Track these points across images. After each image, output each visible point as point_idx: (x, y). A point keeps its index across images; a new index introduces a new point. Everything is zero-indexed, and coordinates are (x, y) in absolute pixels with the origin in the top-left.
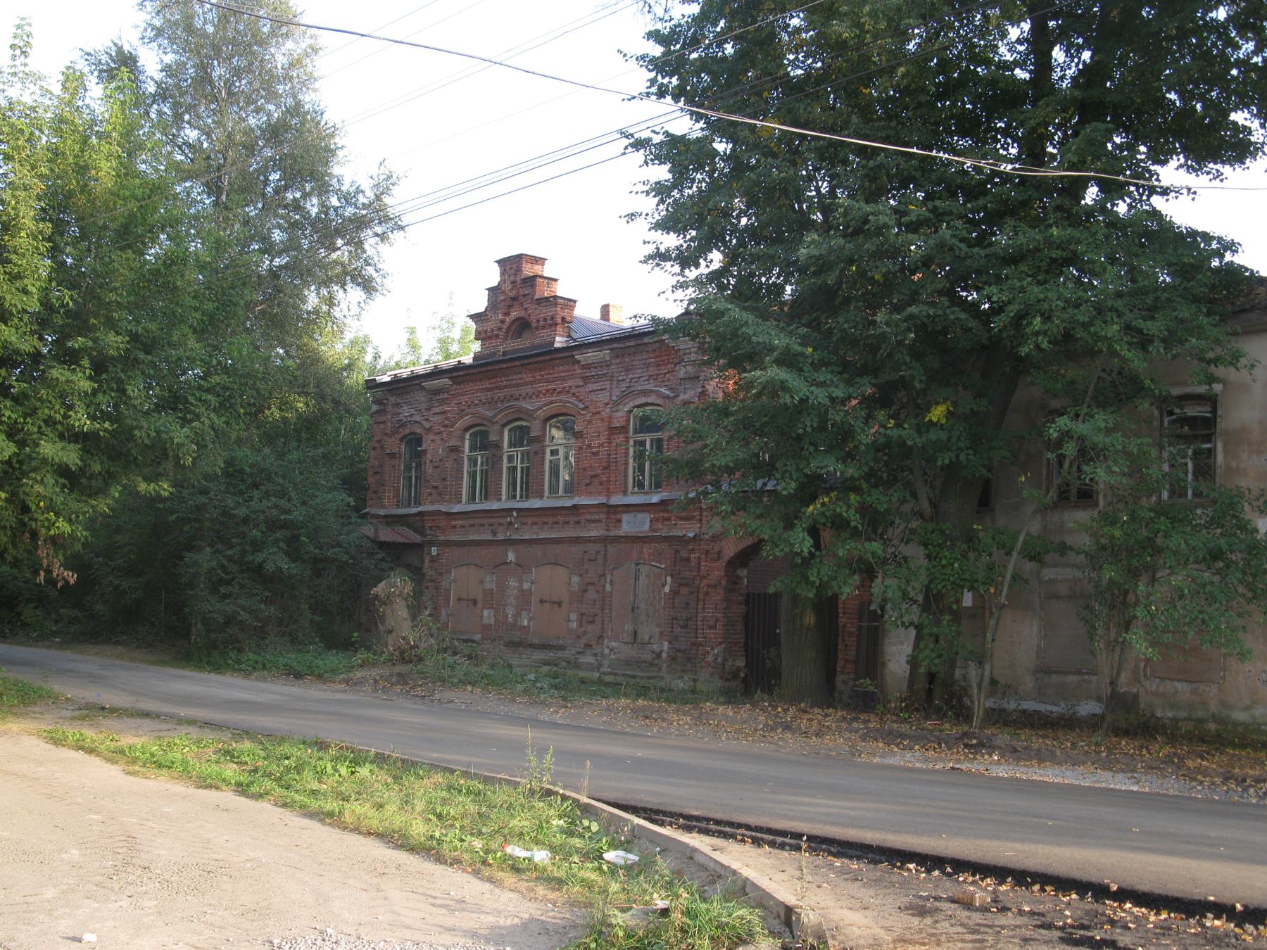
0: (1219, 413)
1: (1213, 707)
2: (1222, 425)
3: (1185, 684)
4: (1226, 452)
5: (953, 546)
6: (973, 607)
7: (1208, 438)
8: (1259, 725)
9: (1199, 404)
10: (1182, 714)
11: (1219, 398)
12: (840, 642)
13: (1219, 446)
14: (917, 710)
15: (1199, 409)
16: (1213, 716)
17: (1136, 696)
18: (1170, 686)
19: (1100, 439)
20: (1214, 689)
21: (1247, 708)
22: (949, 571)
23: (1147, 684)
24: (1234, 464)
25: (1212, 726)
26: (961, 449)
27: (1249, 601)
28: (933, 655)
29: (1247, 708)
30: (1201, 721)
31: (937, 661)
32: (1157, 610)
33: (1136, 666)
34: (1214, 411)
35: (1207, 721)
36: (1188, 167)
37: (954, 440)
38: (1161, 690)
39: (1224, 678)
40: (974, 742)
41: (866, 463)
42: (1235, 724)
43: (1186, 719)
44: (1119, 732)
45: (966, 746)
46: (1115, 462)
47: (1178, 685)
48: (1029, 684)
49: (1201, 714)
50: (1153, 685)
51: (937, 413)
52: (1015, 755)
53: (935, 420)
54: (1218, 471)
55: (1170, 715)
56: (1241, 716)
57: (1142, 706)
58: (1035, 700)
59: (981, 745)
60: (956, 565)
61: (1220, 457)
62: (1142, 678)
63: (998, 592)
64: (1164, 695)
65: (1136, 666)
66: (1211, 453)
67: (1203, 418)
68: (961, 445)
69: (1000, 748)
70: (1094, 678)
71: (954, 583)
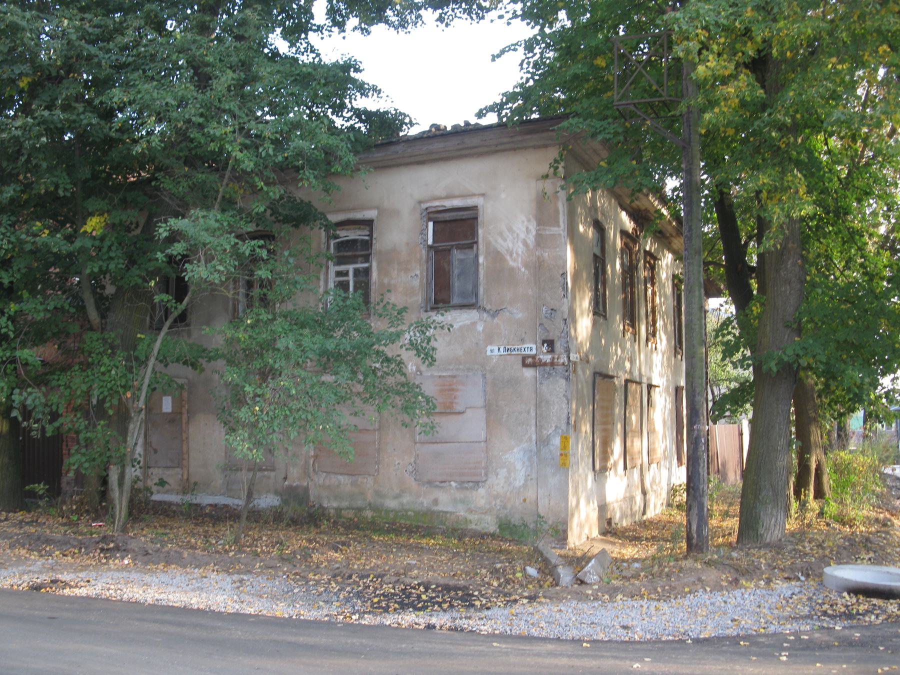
0: (375, 236)
1: (370, 497)
2: (377, 246)
3: (346, 477)
4: (380, 270)
5: (114, 353)
6: (172, 413)
7: (367, 258)
8: (407, 511)
9: (360, 229)
10: (345, 504)
11: (375, 222)
12: (64, 447)
13: (374, 264)
14: (87, 512)
15: (359, 233)
16: (370, 504)
17: (306, 489)
18: (334, 479)
19: (206, 237)
20: (370, 480)
21: (397, 497)
22: (106, 378)
23: (316, 478)
24: (386, 281)
25: (369, 514)
26: (111, 258)
27: (365, 401)
28: (84, 459)
29: (397, 497)
30: (360, 510)
31: (86, 465)
32: (261, 411)
33: (306, 462)
34: (371, 235)
35: (365, 509)
36: (362, 30)
37: (105, 250)
38: (327, 482)
39: (378, 471)
40: (112, 545)
41: (19, 270)
42: (387, 511)
43: (348, 508)
44: (295, 523)
45: (102, 550)
46: (221, 262)
47: (341, 478)
48: (219, 480)
49: (360, 503)
50: (320, 479)
51: (94, 225)
52: (146, 558)
53: (89, 230)
54: (373, 288)
55: (335, 505)
56: (392, 504)
57: (312, 498)
58: (223, 494)
59: (117, 548)
60: (113, 372)
61: (374, 275)
62: (312, 474)
63: (135, 398)
64: (331, 489)
65: (306, 462)
66: (367, 272)
67: (362, 240)
68: (112, 254)
69: (134, 551)
70: (272, 474)
71: (111, 389)
